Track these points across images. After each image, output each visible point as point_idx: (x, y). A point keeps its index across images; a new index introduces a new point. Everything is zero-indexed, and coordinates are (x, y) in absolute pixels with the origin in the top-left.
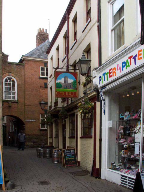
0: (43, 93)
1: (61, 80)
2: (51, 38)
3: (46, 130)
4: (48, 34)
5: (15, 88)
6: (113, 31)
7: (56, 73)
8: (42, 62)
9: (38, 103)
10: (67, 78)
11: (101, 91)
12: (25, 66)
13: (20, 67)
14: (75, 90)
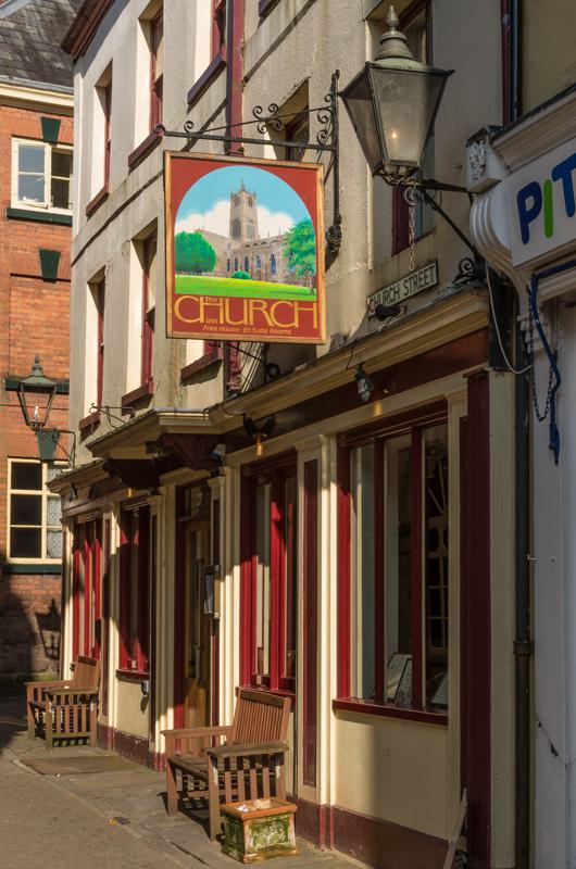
0: (34, 316)
1: (209, 215)
10: (251, 203)
11: (533, 294)
14: (307, 289)
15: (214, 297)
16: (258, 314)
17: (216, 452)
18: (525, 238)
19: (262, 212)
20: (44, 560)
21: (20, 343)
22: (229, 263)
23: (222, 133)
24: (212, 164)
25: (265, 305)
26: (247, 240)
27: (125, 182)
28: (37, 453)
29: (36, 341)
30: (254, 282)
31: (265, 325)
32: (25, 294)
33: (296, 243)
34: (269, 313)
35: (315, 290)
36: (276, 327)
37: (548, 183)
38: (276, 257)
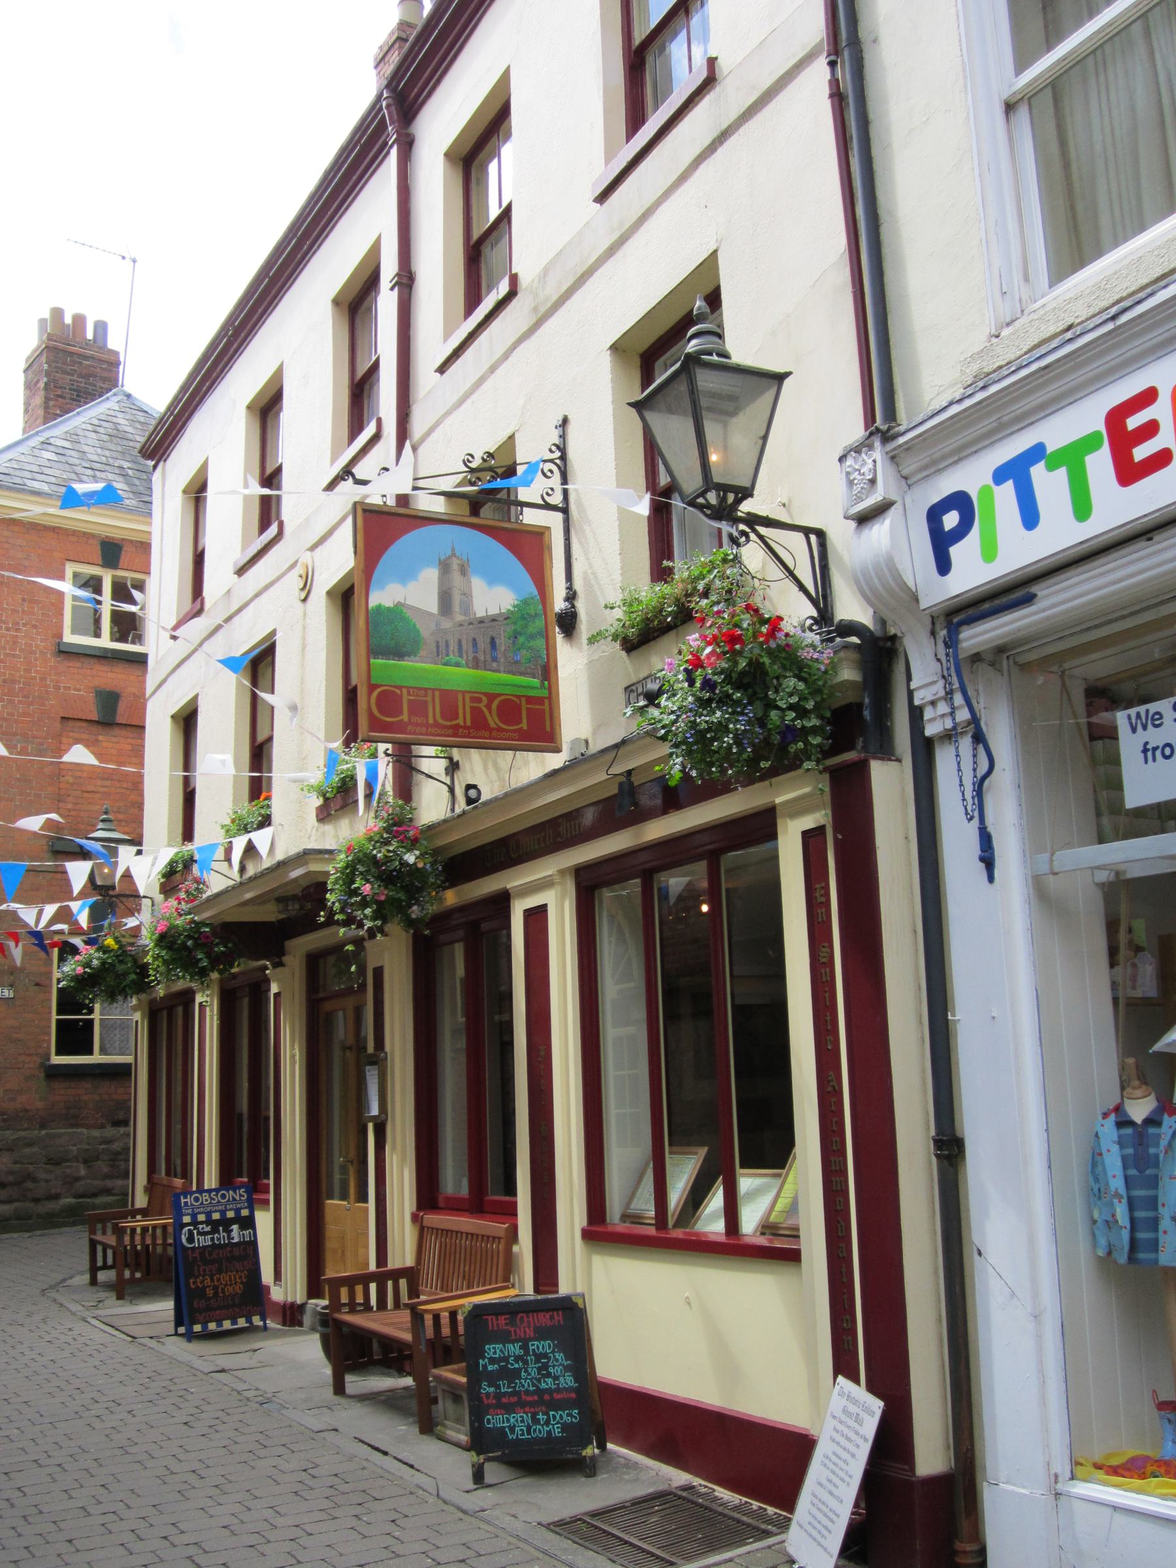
1: (412, 585)
4: (117, 354)
7: (366, 522)
10: (463, 571)
14: (536, 682)
15: (420, 689)
16: (477, 713)
19: (478, 585)
20: (96, 1058)
21: (70, 799)
22: (438, 647)
25: (485, 700)
26: (459, 618)
27: (229, 591)
31: (486, 726)
33: (521, 623)
35: (546, 683)
36: (499, 729)
37: (985, 491)
38: (497, 641)
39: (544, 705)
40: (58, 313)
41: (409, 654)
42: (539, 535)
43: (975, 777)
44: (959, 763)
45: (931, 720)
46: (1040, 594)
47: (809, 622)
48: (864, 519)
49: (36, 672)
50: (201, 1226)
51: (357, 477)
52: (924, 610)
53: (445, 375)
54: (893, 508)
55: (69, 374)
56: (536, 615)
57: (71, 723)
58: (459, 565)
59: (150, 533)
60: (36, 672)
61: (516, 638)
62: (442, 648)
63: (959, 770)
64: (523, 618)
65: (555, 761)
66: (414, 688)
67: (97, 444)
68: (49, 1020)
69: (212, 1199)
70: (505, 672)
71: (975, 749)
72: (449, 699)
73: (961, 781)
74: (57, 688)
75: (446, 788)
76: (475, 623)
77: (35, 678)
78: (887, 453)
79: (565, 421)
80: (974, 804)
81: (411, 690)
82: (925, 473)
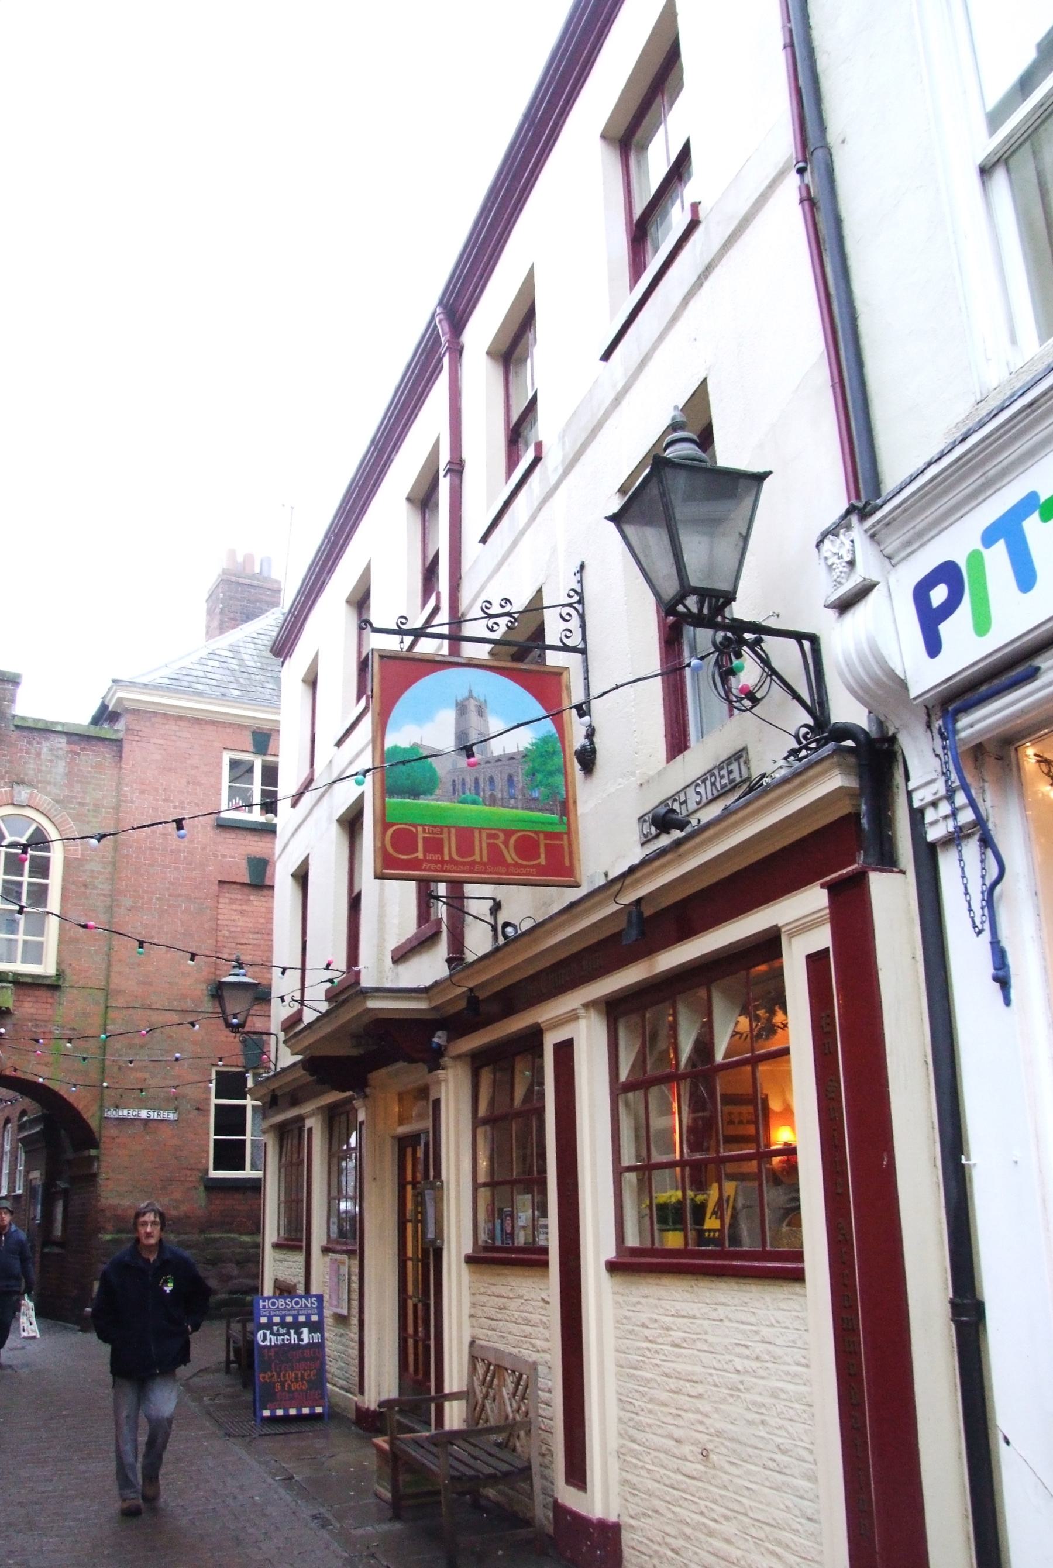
2: (288, 597)
3: (255, 1187)
4: (278, 582)
5: (47, 860)
6: (1000, 177)
8: (236, 726)
9: (201, 990)
10: (481, 712)
12: (127, 747)
13: (90, 758)
14: (554, 817)
16: (493, 849)
17: (436, 1040)
18: (933, 647)
22: (454, 785)
23: (445, 630)
24: (433, 664)
25: (502, 836)
28: (241, 1060)
29: (243, 947)
30: (486, 808)
32: (233, 901)
33: (539, 760)
34: (507, 847)
35: (565, 819)
36: (516, 865)
37: (975, 558)
38: (515, 779)
39: (562, 839)
40: (232, 554)
41: (424, 793)
42: (558, 674)
43: (984, 884)
44: (963, 868)
45: (935, 823)
46: (1044, 666)
47: (804, 730)
48: (844, 605)
49: (198, 842)
50: (275, 1328)
51: (375, 625)
52: (915, 699)
53: (487, 544)
54: (875, 590)
55: (239, 600)
56: (554, 753)
57: (227, 886)
58: (476, 705)
59: (278, 722)
60: (198, 842)
61: (534, 775)
62: (459, 787)
63: (963, 877)
64: (542, 756)
65: (573, 895)
66: (429, 826)
67: (255, 652)
68: (209, 1138)
69: (287, 1304)
70: (523, 808)
71: (983, 853)
72: (465, 836)
73: (966, 888)
74: (215, 856)
75: (490, 927)
76: (493, 761)
77: (197, 848)
78: (866, 531)
79: (582, 567)
80: (983, 915)
81: (427, 828)
82: (909, 550)
